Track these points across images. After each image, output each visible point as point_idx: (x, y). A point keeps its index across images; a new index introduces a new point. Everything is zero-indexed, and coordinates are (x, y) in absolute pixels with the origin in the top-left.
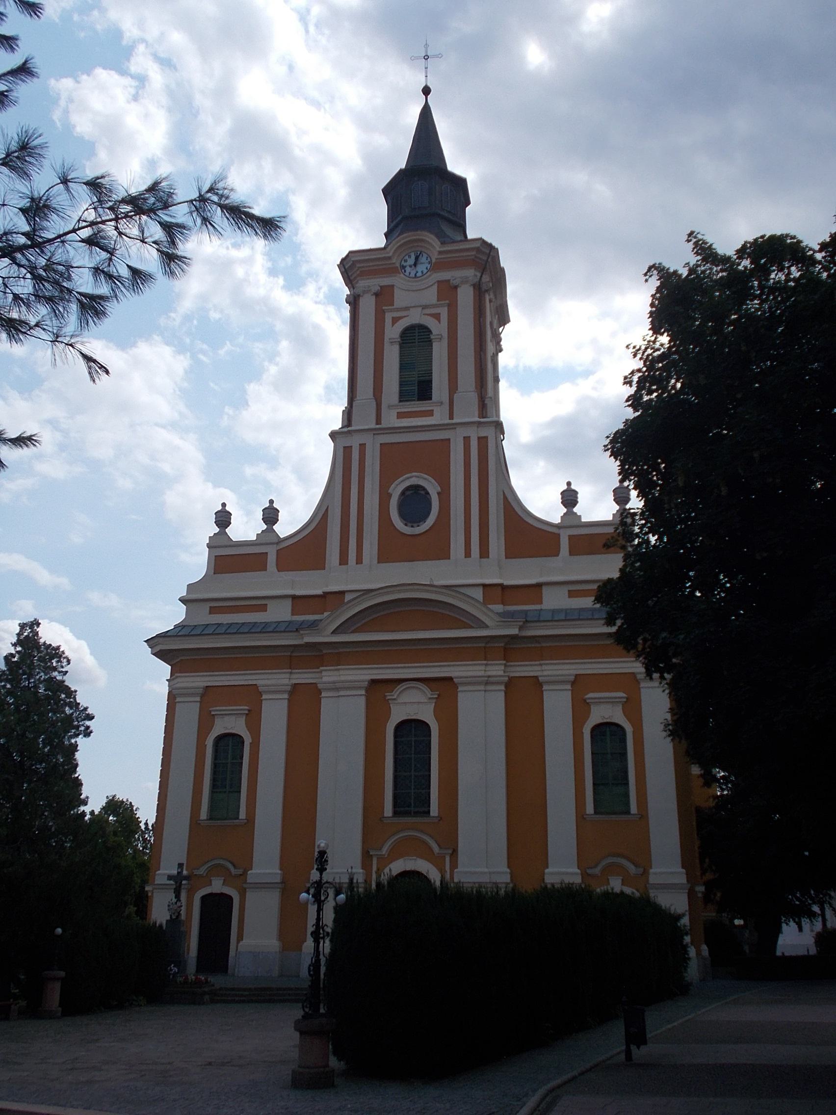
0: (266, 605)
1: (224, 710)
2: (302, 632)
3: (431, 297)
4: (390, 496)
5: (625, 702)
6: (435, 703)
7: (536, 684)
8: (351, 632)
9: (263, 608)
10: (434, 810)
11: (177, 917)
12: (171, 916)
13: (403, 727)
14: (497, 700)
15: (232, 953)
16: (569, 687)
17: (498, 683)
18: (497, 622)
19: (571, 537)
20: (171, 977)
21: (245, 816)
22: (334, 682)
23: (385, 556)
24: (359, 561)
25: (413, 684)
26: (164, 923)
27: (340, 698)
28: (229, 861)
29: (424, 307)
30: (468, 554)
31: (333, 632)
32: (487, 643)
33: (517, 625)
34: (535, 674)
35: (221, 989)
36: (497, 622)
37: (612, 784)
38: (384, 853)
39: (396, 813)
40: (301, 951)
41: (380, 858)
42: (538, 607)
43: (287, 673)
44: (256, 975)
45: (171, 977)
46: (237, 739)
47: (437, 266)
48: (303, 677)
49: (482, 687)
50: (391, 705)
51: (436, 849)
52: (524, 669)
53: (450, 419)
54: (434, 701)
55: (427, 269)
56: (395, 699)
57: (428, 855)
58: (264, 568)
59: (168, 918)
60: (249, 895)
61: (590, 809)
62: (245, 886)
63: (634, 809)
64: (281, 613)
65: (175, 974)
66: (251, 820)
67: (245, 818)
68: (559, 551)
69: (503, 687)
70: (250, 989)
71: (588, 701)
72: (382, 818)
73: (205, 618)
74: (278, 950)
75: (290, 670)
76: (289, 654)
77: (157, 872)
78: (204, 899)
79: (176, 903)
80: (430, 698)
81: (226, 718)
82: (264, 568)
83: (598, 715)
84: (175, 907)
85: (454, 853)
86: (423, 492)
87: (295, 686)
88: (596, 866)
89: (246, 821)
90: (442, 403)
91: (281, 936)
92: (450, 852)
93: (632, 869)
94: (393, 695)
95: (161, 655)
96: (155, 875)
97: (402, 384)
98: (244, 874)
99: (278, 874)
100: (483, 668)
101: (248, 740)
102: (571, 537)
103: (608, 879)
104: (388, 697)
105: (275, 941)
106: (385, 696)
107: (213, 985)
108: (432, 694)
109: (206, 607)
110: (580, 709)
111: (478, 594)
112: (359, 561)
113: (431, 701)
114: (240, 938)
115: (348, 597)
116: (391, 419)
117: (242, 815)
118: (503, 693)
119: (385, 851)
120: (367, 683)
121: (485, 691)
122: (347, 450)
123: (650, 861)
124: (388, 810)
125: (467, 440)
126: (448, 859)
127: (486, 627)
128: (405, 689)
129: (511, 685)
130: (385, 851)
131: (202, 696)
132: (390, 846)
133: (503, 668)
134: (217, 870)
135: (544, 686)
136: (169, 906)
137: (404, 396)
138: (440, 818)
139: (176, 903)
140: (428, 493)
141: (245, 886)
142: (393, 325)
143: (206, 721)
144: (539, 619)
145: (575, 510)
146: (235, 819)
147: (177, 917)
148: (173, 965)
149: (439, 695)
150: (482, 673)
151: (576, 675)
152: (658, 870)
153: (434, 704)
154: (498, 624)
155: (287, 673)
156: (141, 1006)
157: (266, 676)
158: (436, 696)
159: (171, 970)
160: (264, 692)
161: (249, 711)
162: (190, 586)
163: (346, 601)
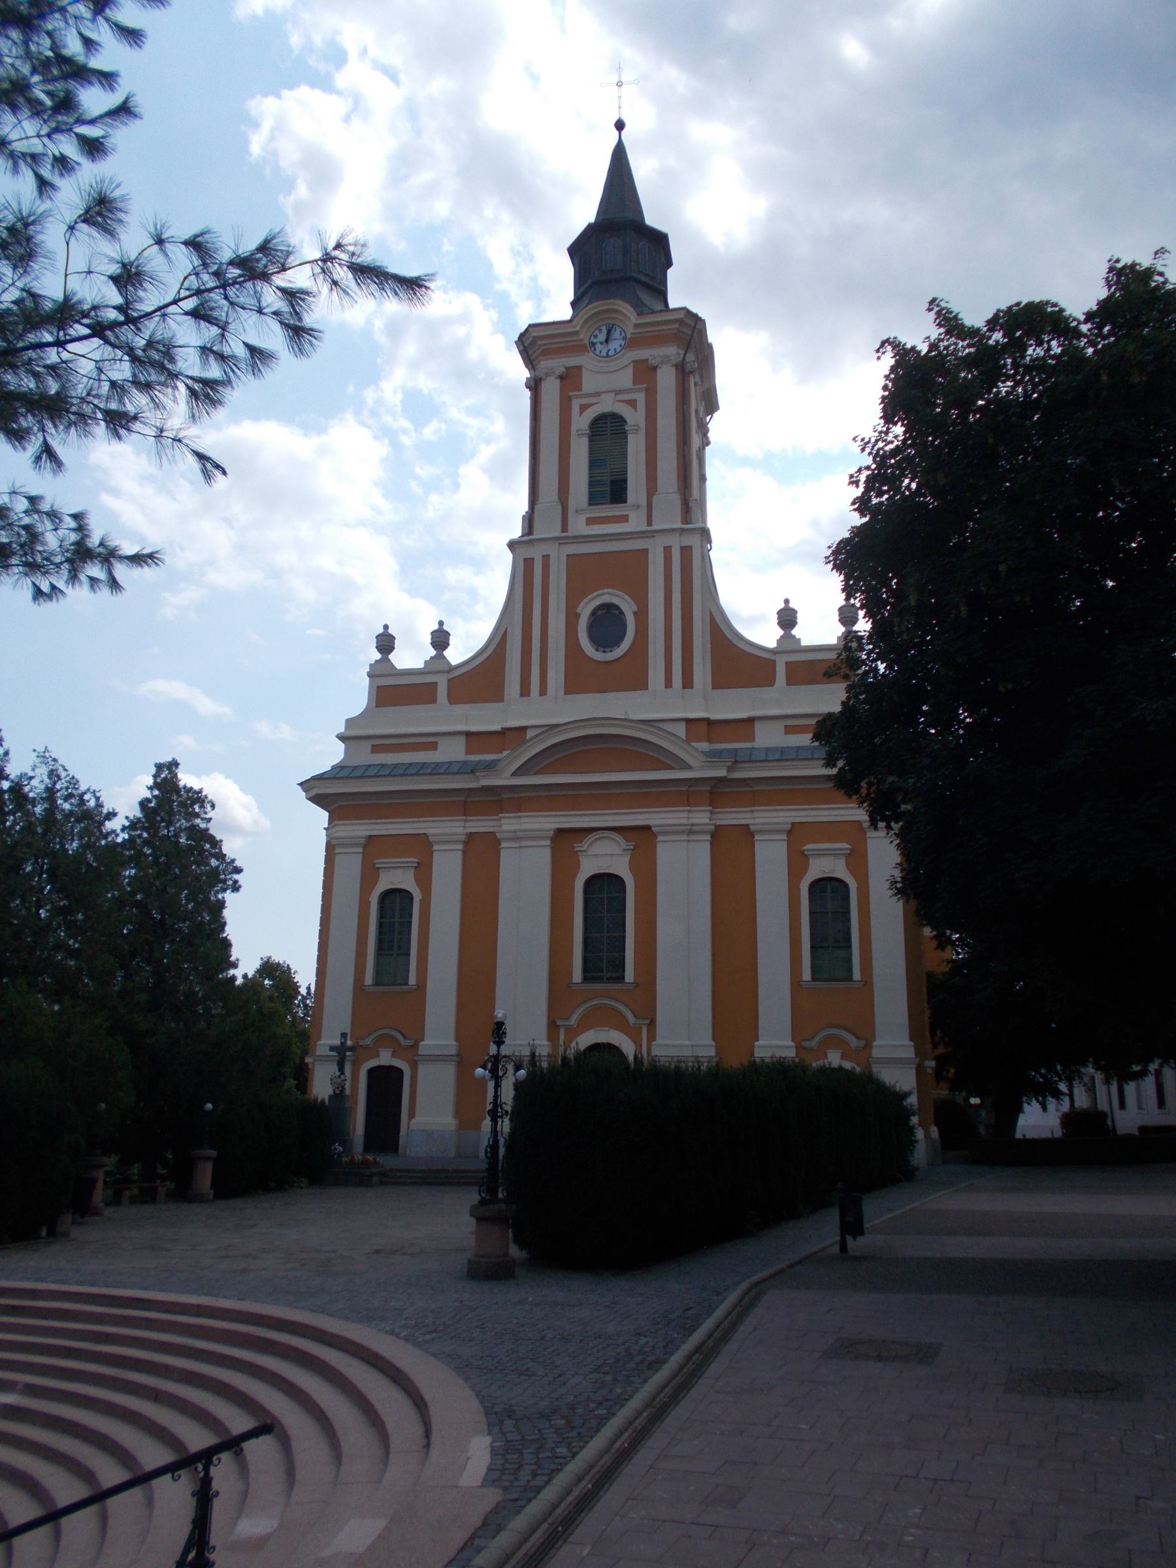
1: (392, 863)
3: (625, 379)
4: (578, 616)
5: (849, 854)
6: (631, 855)
7: (747, 834)
8: (535, 774)
9: (433, 746)
10: (629, 976)
11: (341, 1091)
12: (334, 1090)
13: (595, 882)
14: (701, 853)
16: (784, 837)
17: (704, 832)
24: (543, 691)
25: (614, 835)
29: (618, 392)
30: (668, 684)
31: (515, 774)
32: (689, 787)
35: (391, 1170)
37: (833, 947)
38: (572, 1023)
39: (586, 979)
41: (569, 1029)
42: (748, 745)
43: (462, 820)
45: (336, 1156)
47: (632, 343)
49: (685, 837)
52: (733, 817)
53: (648, 526)
54: (630, 852)
55: (621, 346)
58: (433, 699)
60: (423, 1070)
61: (807, 975)
62: (416, 1058)
63: (857, 975)
64: (453, 751)
65: (340, 1154)
69: (708, 837)
71: (806, 853)
72: (570, 984)
73: (366, 757)
76: (463, 799)
78: (372, 1072)
80: (625, 850)
82: (433, 699)
83: (818, 868)
84: (339, 1081)
85: (652, 1023)
86: (617, 612)
87: (471, 836)
88: (813, 1038)
91: (458, 1113)
92: (647, 1022)
93: (853, 1042)
96: (316, 1046)
97: (591, 484)
98: (415, 1045)
100: (685, 815)
104: (578, 849)
106: (573, 847)
110: (797, 862)
111: (681, 730)
112: (543, 691)
113: (624, 853)
114: (412, 1114)
115: (530, 734)
116: (578, 526)
117: (412, 980)
119: (573, 1021)
122: (528, 563)
124: (577, 975)
125: (668, 550)
127: (688, 767)
129: (718, 835)
130: (573, 1021)
131: (365, 847)
133: (708, 815)
134: (385, 1040)
136: (332, 1080)
137: (594, 499)
138: (636, 984)
139: (339, 1077)
140: (622, 613)
142: (581, 413)
143: (369, 875)
144: (750, 758)
145: (794, 632)
147: (341, 1091)
149: (635, 846)
150: (684, 821)
151: (793, 824)
153: (629, 856)
154: (703, 764)
155: (462, 820)
157: (436, 825)
158: (632, 847)
159: (336, 1149)
162: (350, 722)
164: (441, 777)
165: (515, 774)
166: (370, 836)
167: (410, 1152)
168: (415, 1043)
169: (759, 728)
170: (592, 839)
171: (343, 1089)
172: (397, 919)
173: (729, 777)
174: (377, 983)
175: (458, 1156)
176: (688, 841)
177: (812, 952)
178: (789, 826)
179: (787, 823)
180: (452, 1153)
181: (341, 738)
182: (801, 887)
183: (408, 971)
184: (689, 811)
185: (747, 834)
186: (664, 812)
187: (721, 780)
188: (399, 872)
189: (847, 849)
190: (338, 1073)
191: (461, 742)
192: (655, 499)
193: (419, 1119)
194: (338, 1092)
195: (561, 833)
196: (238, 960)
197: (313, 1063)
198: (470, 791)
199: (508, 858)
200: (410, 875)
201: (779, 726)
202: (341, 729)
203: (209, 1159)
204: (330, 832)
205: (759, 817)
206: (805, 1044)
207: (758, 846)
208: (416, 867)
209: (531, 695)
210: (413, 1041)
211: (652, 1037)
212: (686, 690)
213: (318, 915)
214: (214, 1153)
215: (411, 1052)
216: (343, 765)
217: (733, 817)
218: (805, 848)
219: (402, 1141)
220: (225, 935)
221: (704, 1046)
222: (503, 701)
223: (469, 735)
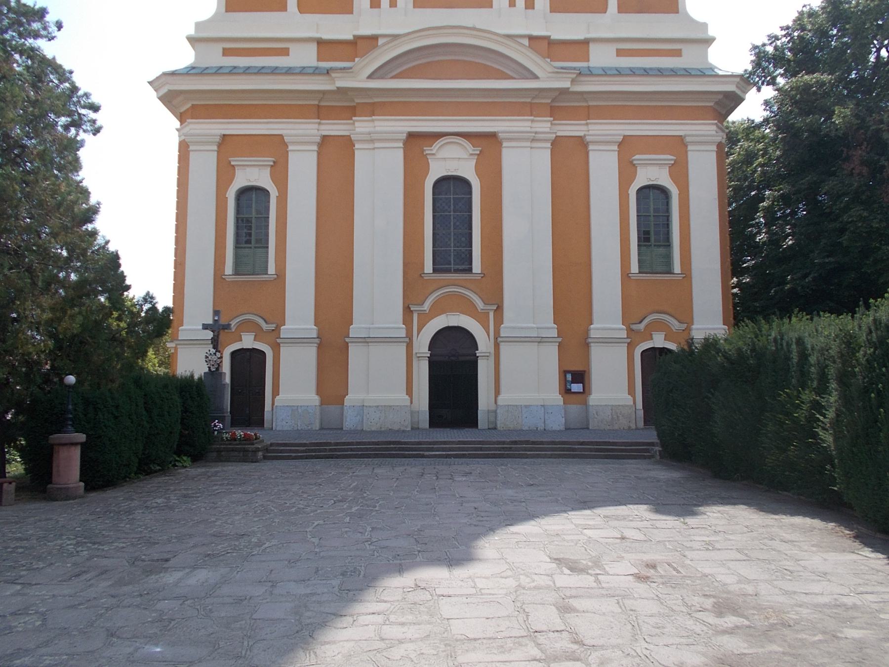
0: (288, 49)
2: (333, 75)
5: (673, 164)
6: (477, 159)
7: (582, 144)
8: (392, 78)
9: (285, 52)
10: (477, 267)
11: (217, 369)
12: (209, 368)
13: (443, 183)
14: (543, 158)
15: (268, 407)
16: (616, 148)
17: (545, 140)
18: (550, 73)
20: (216, 433)
21: (274, 270)
22: (369, 133)
26: (203, 374)
27: (376, 150)
28: (260, 317)
31: (370, 77)
32: (534, 98)
33: (569, 78)
34: (581, 134)
35: (271, 445)
36: (550, 73)
37: (655, 245)
38: (425, 309)
39: (435, 270)
40: (343, 404)
41: (421, 314)
42: (584, 64)
43: (316, 123)
44: (296, 429)
45: (216, 433)
46: (262, 192)
48: (335, 128)
49: (528, 144)
50: (429, 160)
51: (480, 305)
52: (571, 129)
54: (476, 157)
56: (433, 154)
57: (471, 310)
59: (207, 370)
60: (284, 351)
61: (635, 268)
62: (278, 340)
63: (677, 268)
64: (306, 56)
65: (220, 431)
66: (281, 276)
67: (274, 273)
68: (607, 8)
69: (549, 145)
70: (304, 445)
71: (635, 162)
72: (422, 274)
73: (216, 59)
74: (318, 404)
75: (319, 120)
76: (316, 103)
77: (180, 328)
78: (234, 354)
79: (215, 354)
80: (472, 154)
81: (248, 169)
83: (645, 176)
84: (214, 358)
85: (499, 309)
87: (324, 138)
88: (640, 322)
89: (276, 276)
91: (320, 390)
92: (495, 307)
93: (675, 325)
94: (431, 150)
95: (169, 99)
96: (178, 331)
98: (277, 329)
99: (314, 329)
100: (529, 124)
101: (274, 193)
103: (651, 334)
104: (427, 152)
105: (314, 395)
106: (423, 151)
107: (263, 441)
108: (474, 150)
109: (219, 48)
110: (627, 171)
111: (526, 42)
113: (471, 157)
114: (276, 392)
115: (381, 41)
117: (272, 269)
118: (549, 151)
119: (427, 306)
120: (405, 135)
121: (531, 148)
123: (692, 318)
124: (428, 267)
126: (491, 315)
127: (536, 77)
128: (445, 144)
129: (557, 144)
130: (427, 306)
131: (220, 145)
132: (433, 300)
133: (549, 125)
134: (248, 326)
135: (590, 146)
136: (207, 357)
138: (483, 275)
139: (215, 354)
141: (278, 340)
143: (225, 173)
144: (590, 73)
146: (263, 274)
147: (217, 369)
148: (217, 421)
149: (481, 151)
151: (625, 136)
152: (699, 326)
153: (475, 160)
154: (550, 75)
155: (316, 123)
156: (186, 467)
157: (290, 126)
158: (478, 152)
159: (215, 426)
160: (290, 143)
161: (274, 162)
162: (198, 25)
163: (379, 44)
164: (295, 77)
165: (370, 77)
166: (224, 135)
167: (276, 426)
168: (276, 328)
169: (593, 48)
170: (442, 143)
171: (219, 366)
172: (254, 215)
173: (571, 90)
174: (237, 272)
175: (322, 429)
177: (639, 250)
178: (622, 137)
179: (619, 135)
180: (317, 426)
181: (192, 40)
182: (629, 192)
183: (267, 262)
184: (532, 121)
185: (582, 144)
186: (508, 120)
187: (563, 92)
188: (256, 170)
189: (672, 160)
190: (213, 351)
191: (313, 48)
193: (283, 398)
194: (213, 369)
195: (412, 136)
196: (99, 204)
197: (176, 349)
198: (324, 92)
199: (362, 158)
200: (267, 172)
201: (612, 49)
202: (192, 31)
203: (76, 444)
204: (182, 131)
206: (634, 327)
207: (592, 156)
208: (272, 166)
209: (382, 6)
210: (274, 325)
211: (499, 320)
212: (527, 10)
213: (174, 211)
214: (82, 437)
215: (275, 339)
216: (194, 66)
217: (571, 129)
218: (637, 157)
219: (267, 416)
220: (78, 178)
221: (548, 328)
222: (352, 13)
223: (320, 43)
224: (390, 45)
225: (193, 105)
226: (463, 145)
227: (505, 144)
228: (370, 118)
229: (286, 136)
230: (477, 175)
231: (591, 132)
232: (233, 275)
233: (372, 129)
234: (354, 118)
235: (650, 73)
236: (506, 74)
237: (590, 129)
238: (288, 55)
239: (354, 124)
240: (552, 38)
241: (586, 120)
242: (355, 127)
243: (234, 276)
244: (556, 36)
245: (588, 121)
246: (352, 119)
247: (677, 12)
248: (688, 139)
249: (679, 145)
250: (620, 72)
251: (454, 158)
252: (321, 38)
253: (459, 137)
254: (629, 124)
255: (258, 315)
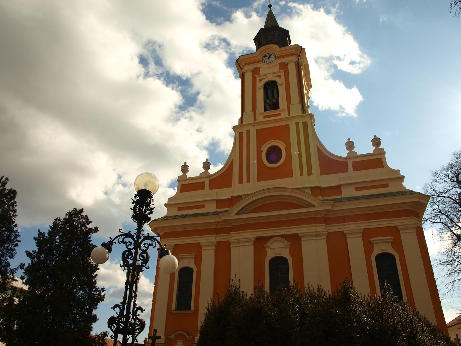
3: (277, 69)
9: (387, 186)
16: (361, 235)
19: (353, 163)
22: (237, 239)
23: (261, 177)
24: (248, 181)
30: (302, 174)
31: (237, 214)
34: (342, 230)
43: (214, 236)
47: (277, 58)
49: (314, 238)
50: (267, 250)
54: (289, 246)
55: (274, 59)
64: (211, 208)
71: (372, 242)
73: (176, 212)
75: (215, 235)
76: (215, 227)
80: (287, 245)
83: (378, 249)
90: (284, 110)
94: (267, 245)
100: (314, 228)
102: (353, 163)
106: (264, 245)
108: (288, 243)
110: (368, 247)
111: (309, 191)
116: (260, 118)
117: (192, 307)
122: (241, 134)
129: (330, 237)
150: (313, 231)
151: (364, 229)
153: (289, 248)
158: (290, 244)
161: (196, 255)
170: (272, 241)
173: (332, 210)
176: (316, 239)
178: (363, 230)
184: (315, 226)
185: (343, 235)
187: (329, 211)
189: (391, 239)
192: (291, 107)
198: (218, 222)
199: (235, 252)
205: (349, 227)
223: (218, 201)
224: (246, 199)
225: (164, 233)
226: (280, 240)
227: (302, 239)
228: (342, 224)
229: (201, 243)
230: (290, 255)
231: (347, 229)
232: (175, 310)
233: (239, 237)
234: (231, 233)
235: (393, 195)
236: (303, 206)
237: (346, 227)
238: (389, 187)
239: (231, 235)
240: (322, 186)
241: (238, 231)
242: (231, 237)
243: (175, 311)
244: (324, 185)
245: (344, 223)
246: (230, 233)
247: (383, 167)
248: (399, 228)
249: (395, 231)
250: (355, 198)
251: (279, 248)
252: (218, 199)
253: (277, 237)
254: (372, 222)
255: (185, 332)
